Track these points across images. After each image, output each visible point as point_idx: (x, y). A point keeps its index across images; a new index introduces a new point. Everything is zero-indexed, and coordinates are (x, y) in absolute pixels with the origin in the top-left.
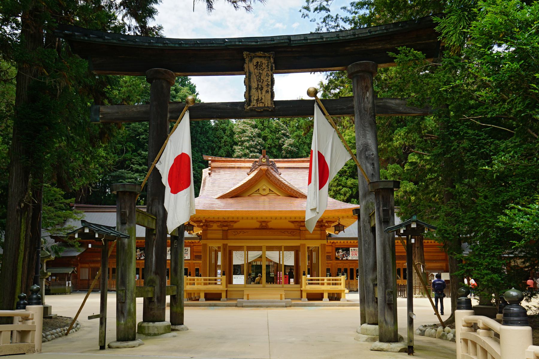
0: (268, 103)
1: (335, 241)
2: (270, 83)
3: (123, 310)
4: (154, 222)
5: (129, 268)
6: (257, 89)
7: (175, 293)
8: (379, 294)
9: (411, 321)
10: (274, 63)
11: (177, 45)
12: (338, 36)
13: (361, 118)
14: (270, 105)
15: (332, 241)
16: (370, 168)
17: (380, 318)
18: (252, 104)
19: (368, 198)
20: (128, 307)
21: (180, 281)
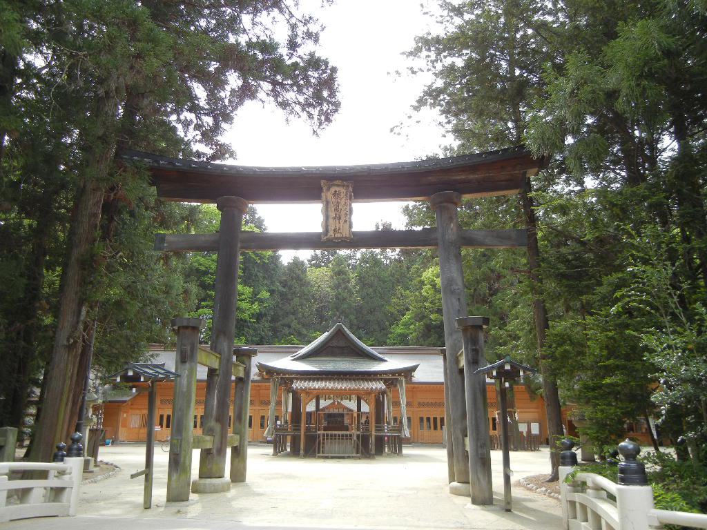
0: (346, 234)
1: (416, 386)
2: (348, 213)
4: (218, 360)
6: (335, 218)
15: (413, 386)
18: (329, 234)
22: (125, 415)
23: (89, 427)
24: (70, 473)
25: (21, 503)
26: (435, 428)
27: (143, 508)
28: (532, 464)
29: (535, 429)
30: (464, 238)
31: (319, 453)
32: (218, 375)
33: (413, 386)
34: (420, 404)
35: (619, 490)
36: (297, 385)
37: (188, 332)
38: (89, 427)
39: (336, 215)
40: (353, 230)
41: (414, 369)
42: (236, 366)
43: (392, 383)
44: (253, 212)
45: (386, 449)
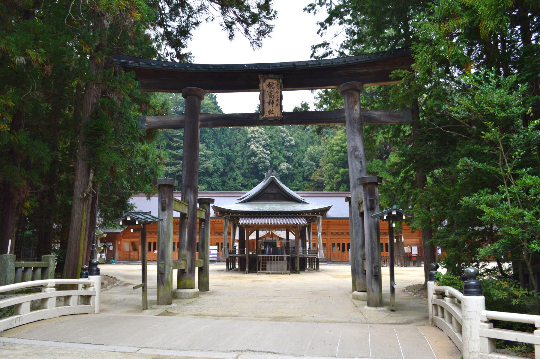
0: (278, 114)
1: (330, 220)
2: (279, 99)
4: (187, 208)
5: (167, 246)
6: (269, 103)
7: (202, 265)
8: (367, 268)
9: (393, 289)
10: (283, 83)
11: (207, 70)
12: (332, 63)
13: (351, 125)
14: (279, 116)
15: (327, 220)
16: (359, 165)
17: (368, 288)
18: (265, 115)
19: (357, 189)
20: (166, 277)
21: (206, 256)
22: (119, 243)
25: (64, 305)
28: (411, 275)
29: (415, 251)
30: (365, 117)
31: (259, 270)
32: (187, 218)
33: (327, 220)
34: (333, 234)
36: (242, 221)
37: (166, 189)
39: (271, 100)
41: (328, 209)
43: (312, 220)
45: (308, 266)
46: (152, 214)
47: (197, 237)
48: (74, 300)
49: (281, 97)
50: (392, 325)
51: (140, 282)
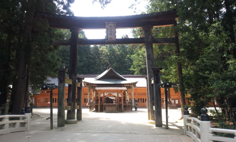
0: (114, 40)
3: (60, 114)
4: (72, 82)
6: (110, 34)
7: (78, 108)
18: (108, 40)
22: (39, 99)
23: (29, 103)
24: (27, 118)
25: (13, 127)
26: (143, 102)
27: (50, 129)
31: (104, 111)
35: (201, 122)
36: (97, 89)
38: (29, 103)
40: (116, 38)
41: (136, 83)
42: (78, 83)
43: (129, 88)
44: (83, 33)
46: (55, 84)
47: (76, 96)
48: (18, 125)
49: (116, 32)
50: (167, 135)
51: (49, 116)
